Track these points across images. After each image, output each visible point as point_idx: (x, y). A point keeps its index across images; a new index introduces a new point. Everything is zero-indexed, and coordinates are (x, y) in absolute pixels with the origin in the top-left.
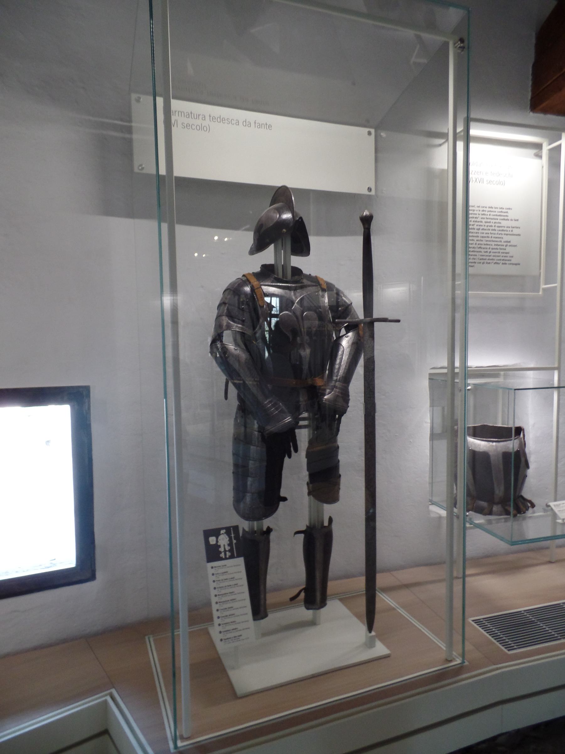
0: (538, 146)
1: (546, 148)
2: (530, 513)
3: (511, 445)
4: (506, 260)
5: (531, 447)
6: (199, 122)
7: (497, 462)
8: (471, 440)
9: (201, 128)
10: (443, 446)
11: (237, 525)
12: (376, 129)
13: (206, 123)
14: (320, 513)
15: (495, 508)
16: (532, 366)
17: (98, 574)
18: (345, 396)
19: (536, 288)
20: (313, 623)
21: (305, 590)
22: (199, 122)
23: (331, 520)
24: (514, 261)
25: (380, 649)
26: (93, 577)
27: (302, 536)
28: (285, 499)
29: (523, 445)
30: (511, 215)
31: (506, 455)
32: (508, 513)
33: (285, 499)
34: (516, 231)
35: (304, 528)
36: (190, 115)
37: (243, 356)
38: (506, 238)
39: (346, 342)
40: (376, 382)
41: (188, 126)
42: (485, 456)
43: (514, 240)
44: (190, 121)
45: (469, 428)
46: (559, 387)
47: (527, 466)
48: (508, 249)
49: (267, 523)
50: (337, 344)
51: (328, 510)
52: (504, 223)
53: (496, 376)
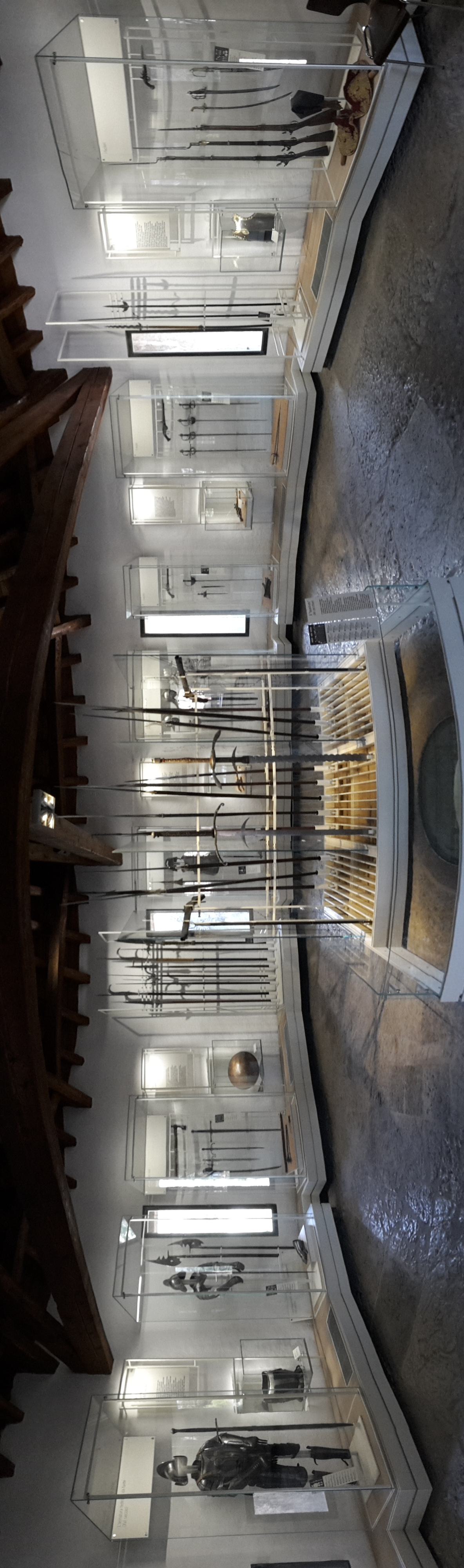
0: (128, 1370)
1: (130, 1367)
2: (302, 1368)
3: (271, 1376)
4: (182, 1382)
5: (272, 1368)
6: (123, 1512)
7: (278, 1382)
8: (270, 1392)
9: (126, 1510)
10: (273, 1406)
11: (296, 1442)
12: (124, 1436)
13: (124, 1509)
14: (306, 1452)
15: (301, 1382)
16: (232, 1369)
17: (346, 1559)
18: (250, 1438)
19: (196, 1369)
20: (357, 1454)
21: (342, 1459)
22: (123, 1512)
23: (308, 1447)
24: (183, 1378)
25: (360, 1421)
26: (348, 1562)
27: (317, 1460)
28: (298, 1465)
29: (271, 1372)
30: (161, 1380)
31: (275, 1378)
32: (302, 1376)
33: (298, 1465)
34: (169, 1378)
35: (312, 1460)
36: (121, 1516)
37: (235, 1479)
38: (172, 1382)
39: (226, 1442)
40: (271, 124)
41: (126, 1516)
42: (276, 1387)
43: (173, 1379)
44: (123, 1515)
45: (144, 483)
46: (242, 1358)
47: (280, 1369)
48: (177, 1381)
49: (310, 1473)
50: (228, 1445)
51: (303, 1448)
52: (165, 1383)
53: (238, 1385)
